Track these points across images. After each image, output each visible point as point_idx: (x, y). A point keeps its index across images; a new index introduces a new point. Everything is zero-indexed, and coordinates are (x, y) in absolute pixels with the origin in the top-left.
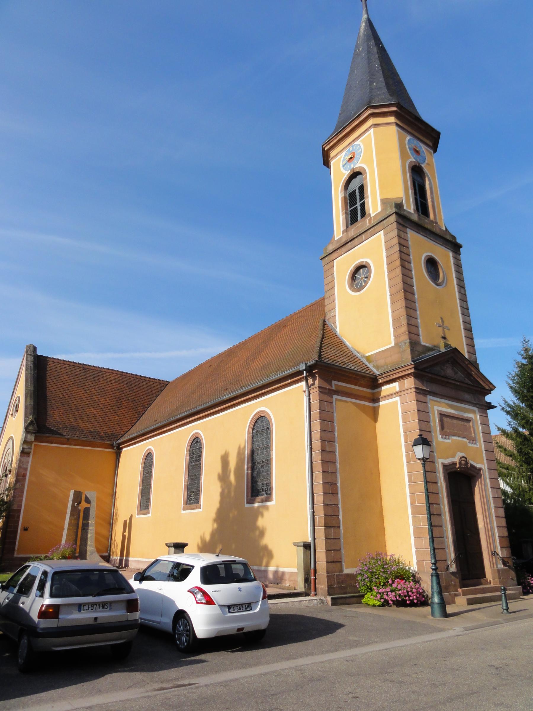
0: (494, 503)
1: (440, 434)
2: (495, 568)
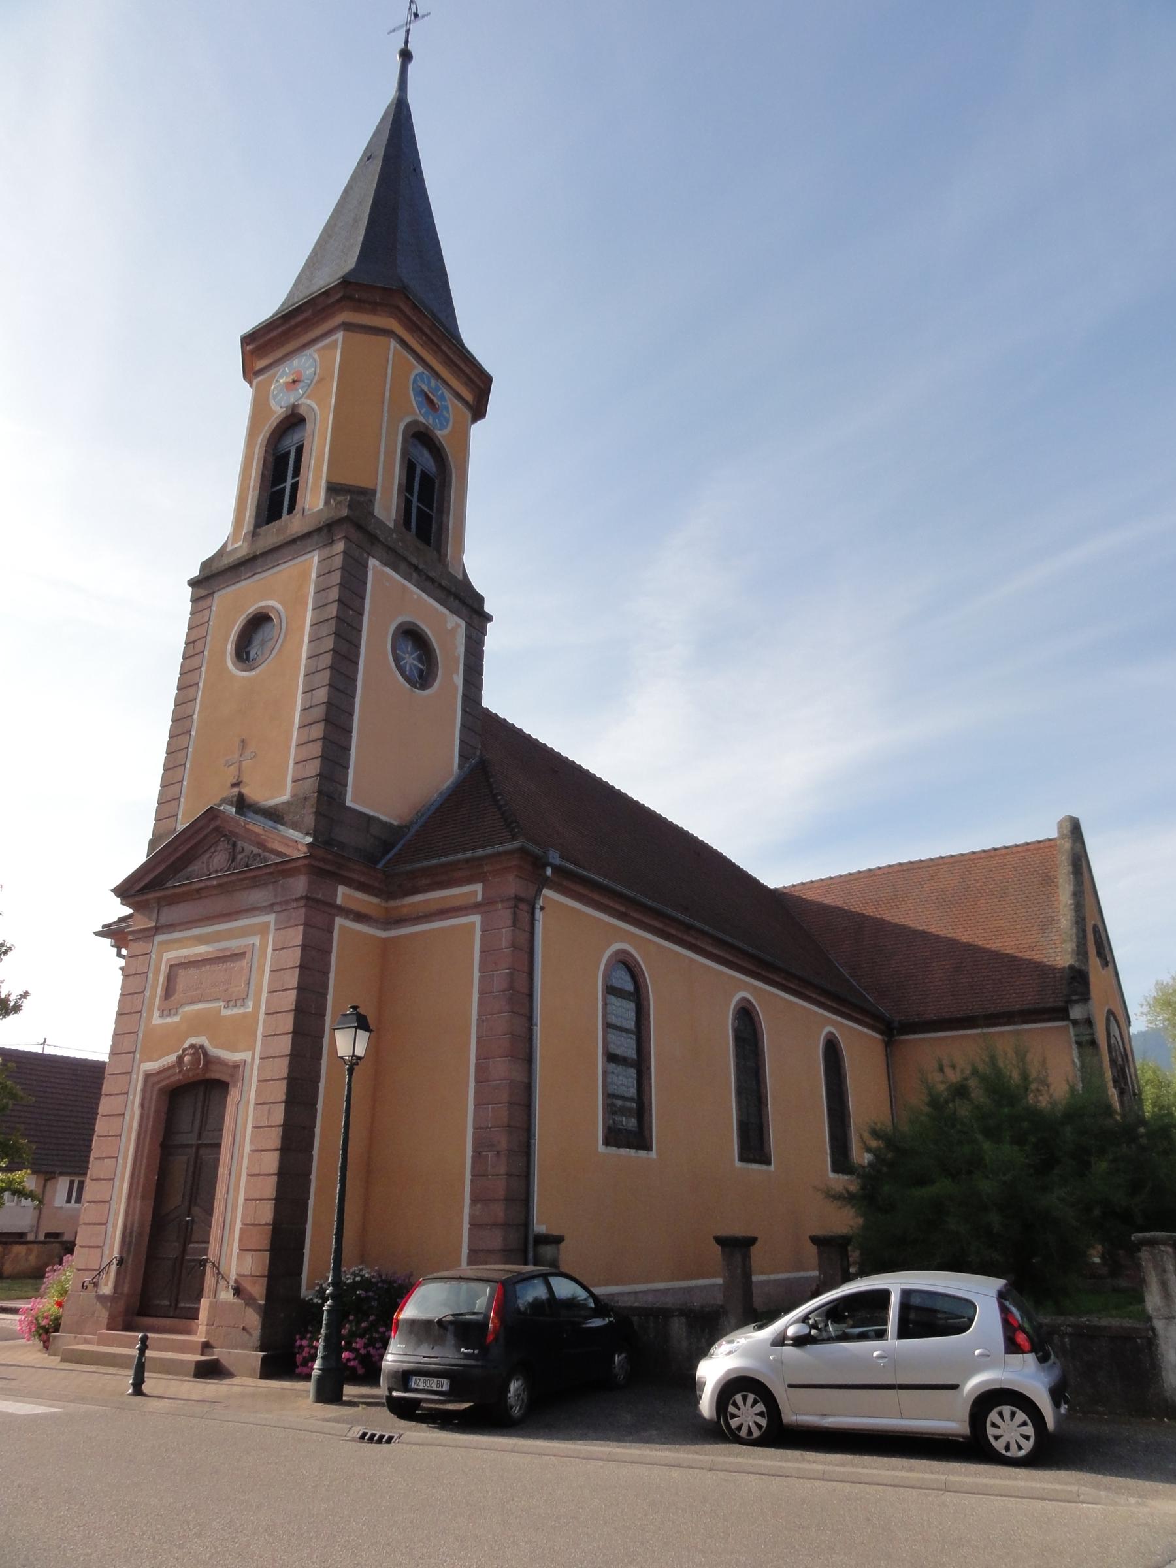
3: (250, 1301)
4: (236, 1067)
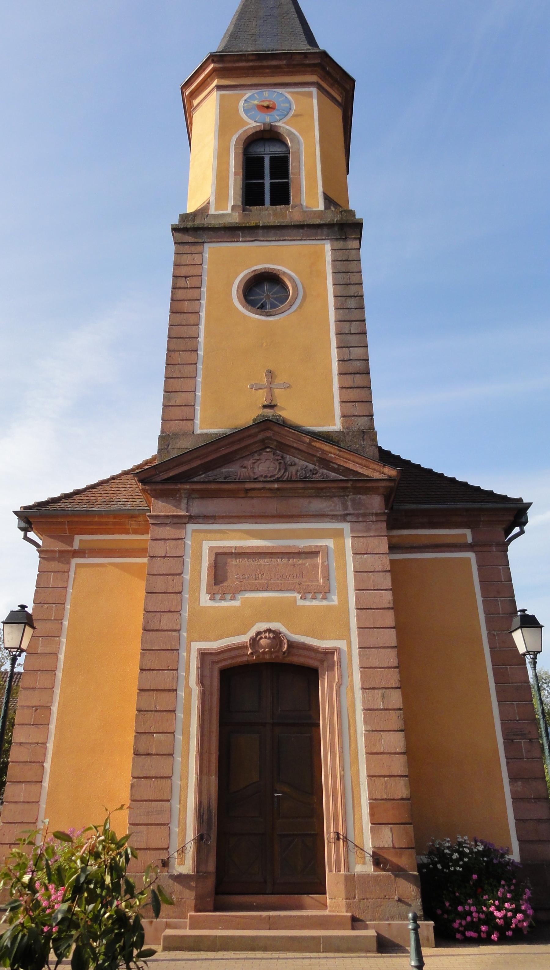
0: (365, 723)
1: (208, 593)
2: (343, 872)
3: (399, 872)
4: (329, 653)
